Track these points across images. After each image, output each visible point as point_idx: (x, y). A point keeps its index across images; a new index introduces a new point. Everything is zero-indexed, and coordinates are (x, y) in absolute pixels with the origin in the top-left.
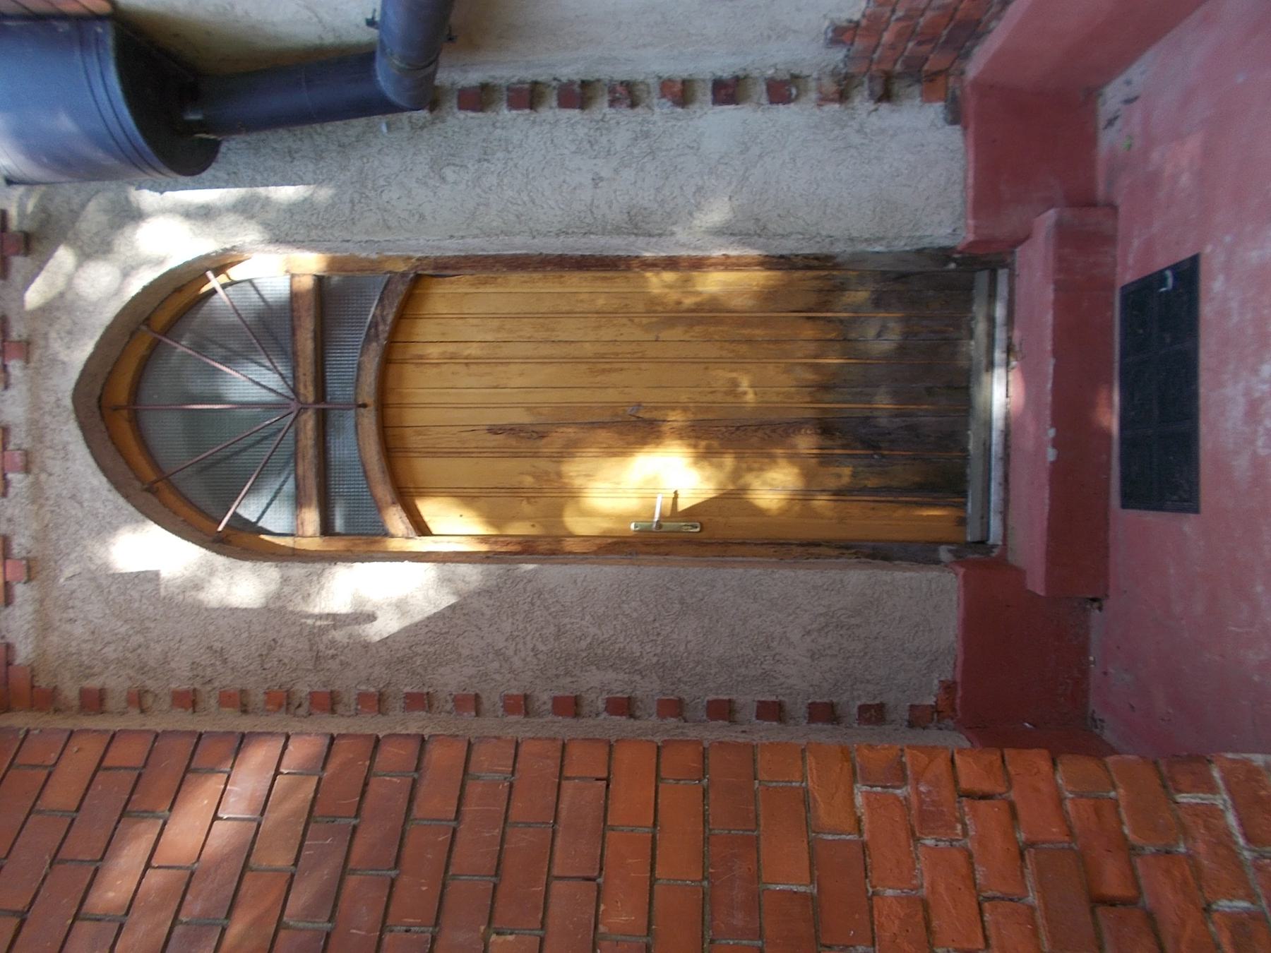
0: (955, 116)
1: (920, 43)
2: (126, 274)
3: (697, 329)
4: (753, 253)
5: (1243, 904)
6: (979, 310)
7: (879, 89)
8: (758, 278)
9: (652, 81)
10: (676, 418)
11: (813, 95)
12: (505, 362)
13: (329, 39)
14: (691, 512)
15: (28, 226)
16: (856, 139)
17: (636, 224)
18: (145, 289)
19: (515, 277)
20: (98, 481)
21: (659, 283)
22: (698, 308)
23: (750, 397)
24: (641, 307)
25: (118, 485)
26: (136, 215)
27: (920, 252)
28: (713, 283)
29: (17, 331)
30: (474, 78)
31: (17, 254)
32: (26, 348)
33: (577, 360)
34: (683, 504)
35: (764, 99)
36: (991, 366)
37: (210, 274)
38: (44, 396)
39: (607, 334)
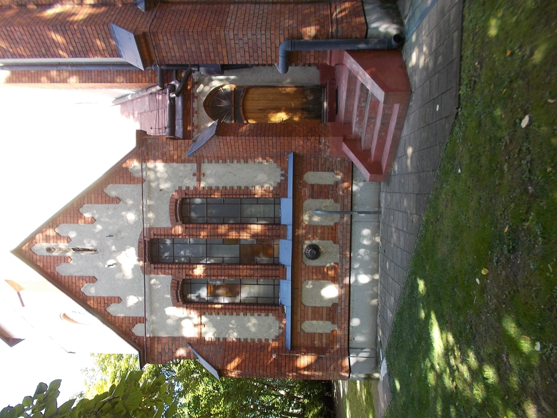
2: (211, 88)
4: (293, 86)
5: (506, 170)
6: (323, 95)
8: (294, 89)
10: (283, 109)
14: (285, 121)
17: (278, 81)
19: (261, 89)
20: (206, 115)
23: (293, 105)
25: (209, 115)
26: (212, 80)
27: (315, 85)
28: (288, 90)
29: (195, 95)
32: (197, 97)
34: (284, 120)
36: (324, 101)
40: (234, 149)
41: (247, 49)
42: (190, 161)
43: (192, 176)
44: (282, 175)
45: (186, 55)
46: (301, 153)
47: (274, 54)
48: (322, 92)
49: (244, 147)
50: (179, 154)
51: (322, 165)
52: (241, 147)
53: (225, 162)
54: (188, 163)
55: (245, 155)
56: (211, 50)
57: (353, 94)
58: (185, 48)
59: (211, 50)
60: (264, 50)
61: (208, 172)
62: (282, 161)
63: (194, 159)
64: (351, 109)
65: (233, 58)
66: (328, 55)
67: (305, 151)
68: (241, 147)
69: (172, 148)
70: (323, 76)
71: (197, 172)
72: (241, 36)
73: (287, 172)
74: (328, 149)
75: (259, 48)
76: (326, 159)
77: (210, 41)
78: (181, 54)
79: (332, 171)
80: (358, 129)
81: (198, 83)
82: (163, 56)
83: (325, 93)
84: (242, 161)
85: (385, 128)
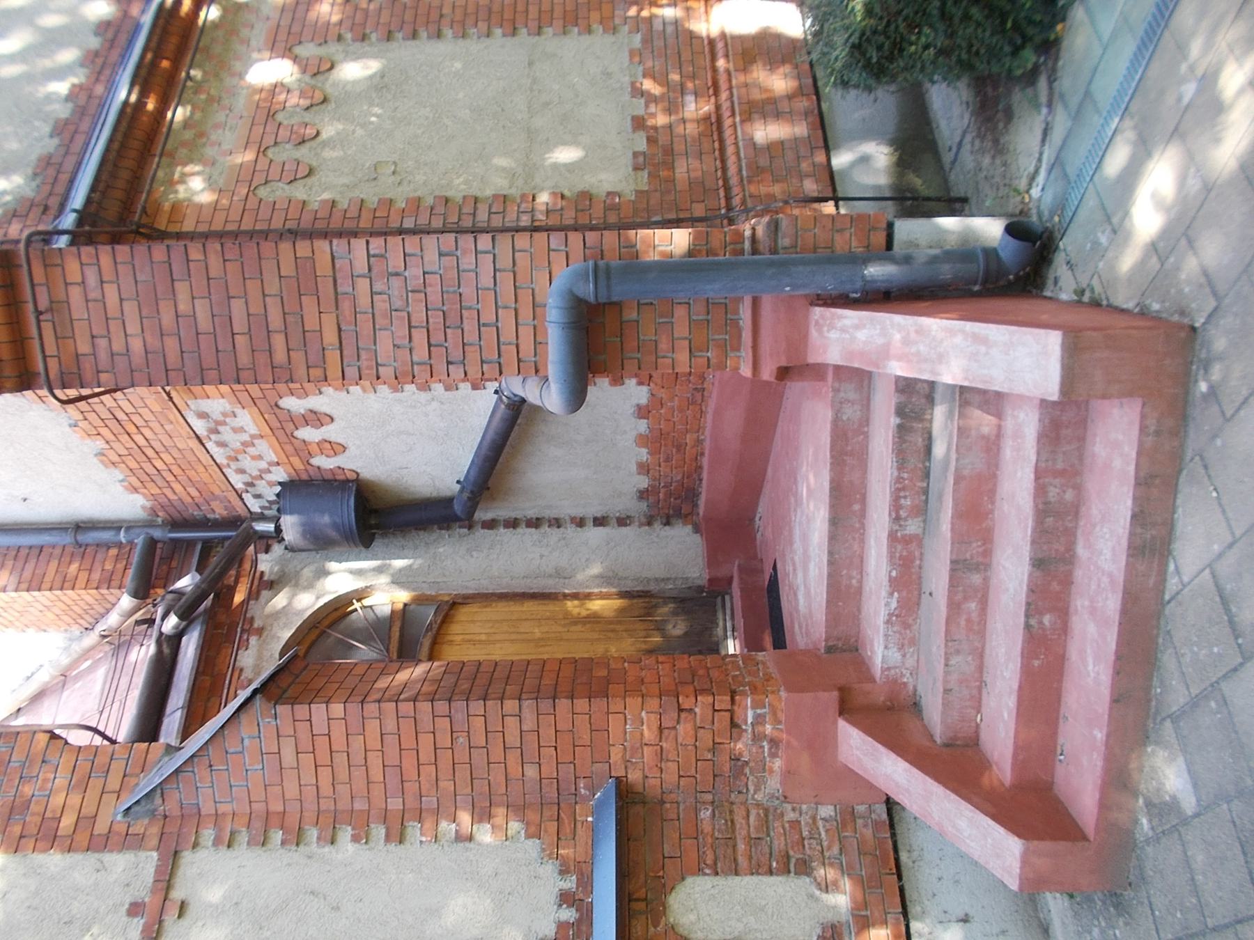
0: (697, 529)
1: (675, 499)
2: (318, 598)
3: (588, 626)
4: (614, 590)
6: (720, 616)
7: (664, 521)
8: (617, 603)
9: (567, 518)
11: (637, 524)
12: (494, 642)
13: (435, 494)
15: (272, 578)
16: (656, 540)
17: (559, 574)
18: (325, 604)
21: (571, 605)
22: (588, 617)
24: (561, 616)
26: (327, 573)
27: (690, 588)
28: (596, 605)
30: (489, 516)
31: (266, 589)
32: (260, 632)
33: (529, 641)
35: (616, 525)
36: (726, 638)
37: (354, 601)
38: (265, 653)
39: (545, 629)
40: (343, 775)
41: (419, 316)
42: (130, 842)
43: (125, 919)
44: (566, 898)
45: (171, 344)
46: (652, 782)
47: (526, 333)
48: (715, 612)
49: (392, 758)
50: (88, 810)
51: (752, 841)
52: (375, 761)
53: (296, 838)
54: (120, 851)
55: (395, 804)
56: (275, 320)
57: (856, 507)
58: (167, 319)
59: (275, 320)
60: (489, 316)
61: (214, 894)
62: (567, 829)
63: (155, 830)
64: (854, 582)
65: (363, 355)
66: (747, 336)
67: (671, 776)
68: (375, 761)
69: (61, 781)
70: (714, 554)
71: (153, 891)
72: (395, 262)
73: (586, 882)
74: (773, 755)
75: (470, 308)
76: (766, 811)
77: (273, 287)
78: (153, 342)
79: (804, 868)
80: (898, 656)
81: (273, 585)
82: (77, 355)
83: (728, 612)
84: (379, 831)
85: (1055, 586)
